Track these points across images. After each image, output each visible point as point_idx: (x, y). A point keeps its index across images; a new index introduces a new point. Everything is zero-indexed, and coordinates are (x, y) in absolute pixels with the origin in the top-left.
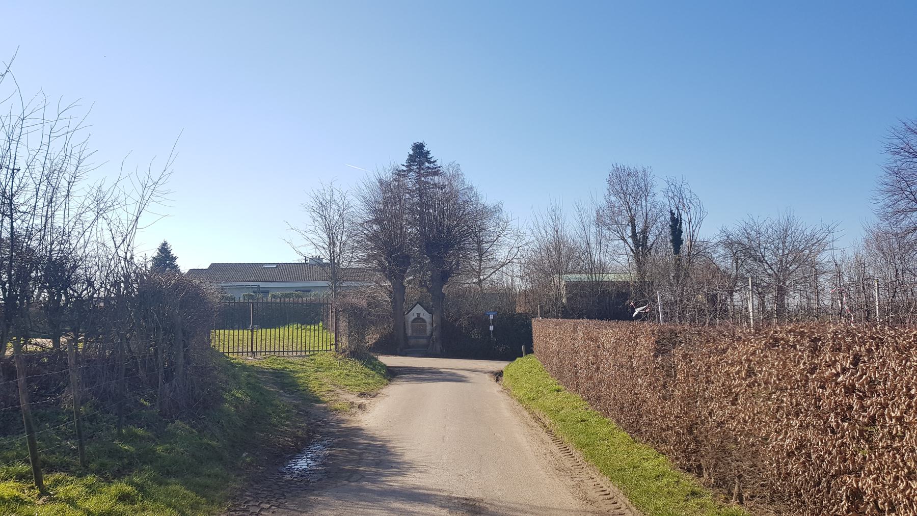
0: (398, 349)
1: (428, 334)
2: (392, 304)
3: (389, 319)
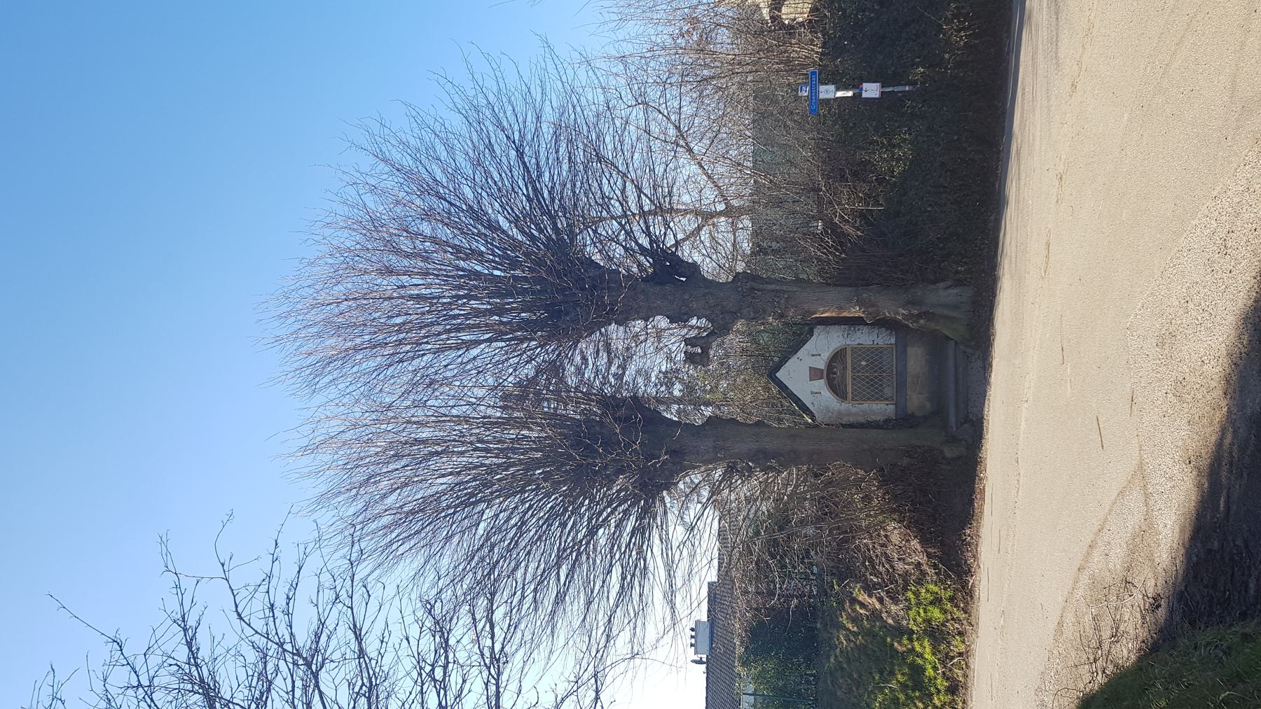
0: (949, 452)
1: (883, 339)
2: (772, 469)
3: (830, 483)
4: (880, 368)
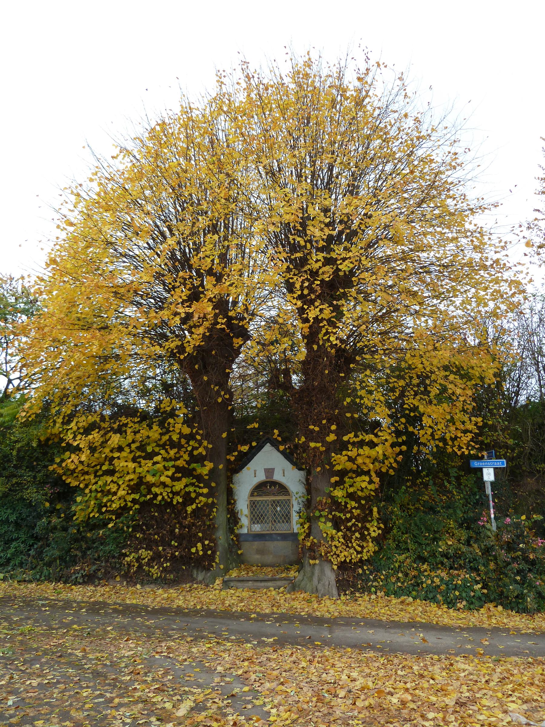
4: (275, 521)
